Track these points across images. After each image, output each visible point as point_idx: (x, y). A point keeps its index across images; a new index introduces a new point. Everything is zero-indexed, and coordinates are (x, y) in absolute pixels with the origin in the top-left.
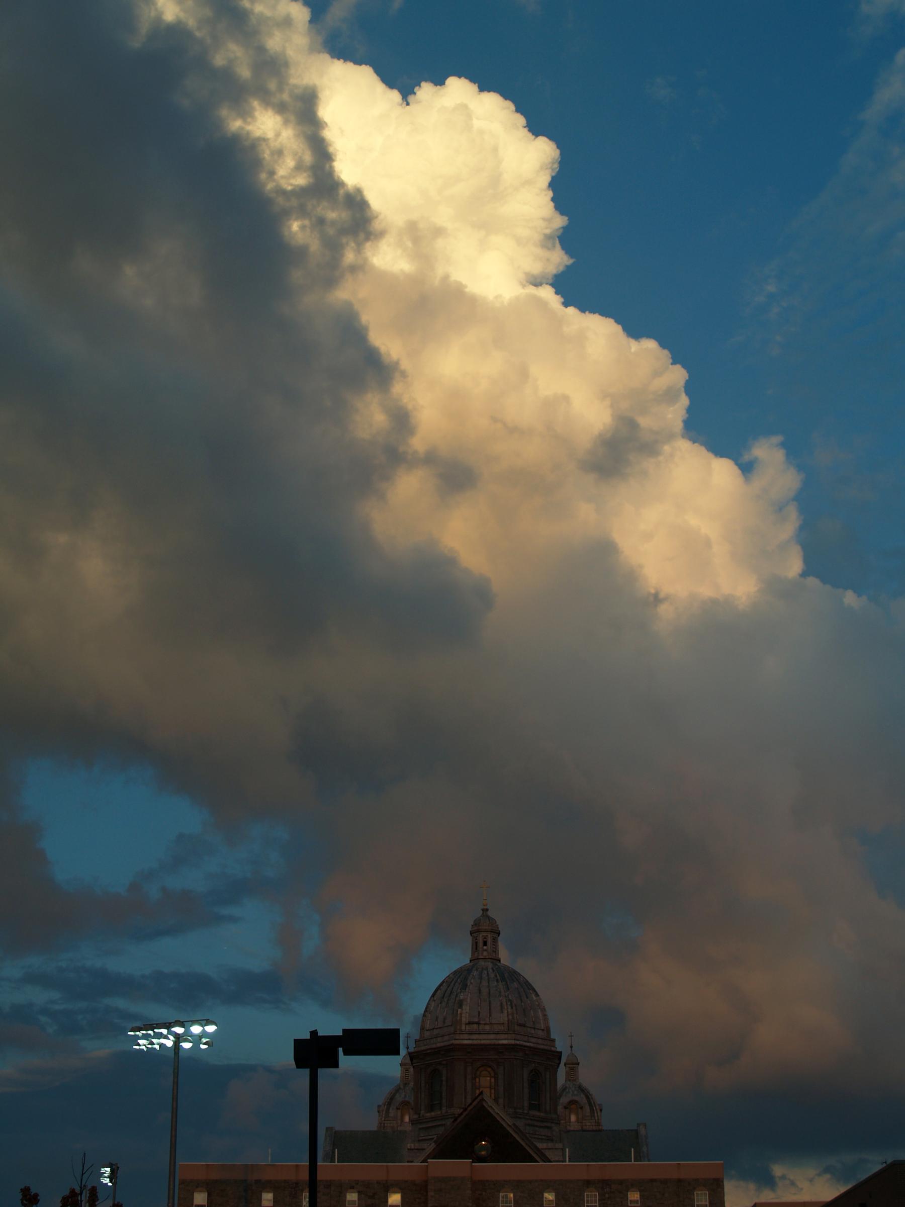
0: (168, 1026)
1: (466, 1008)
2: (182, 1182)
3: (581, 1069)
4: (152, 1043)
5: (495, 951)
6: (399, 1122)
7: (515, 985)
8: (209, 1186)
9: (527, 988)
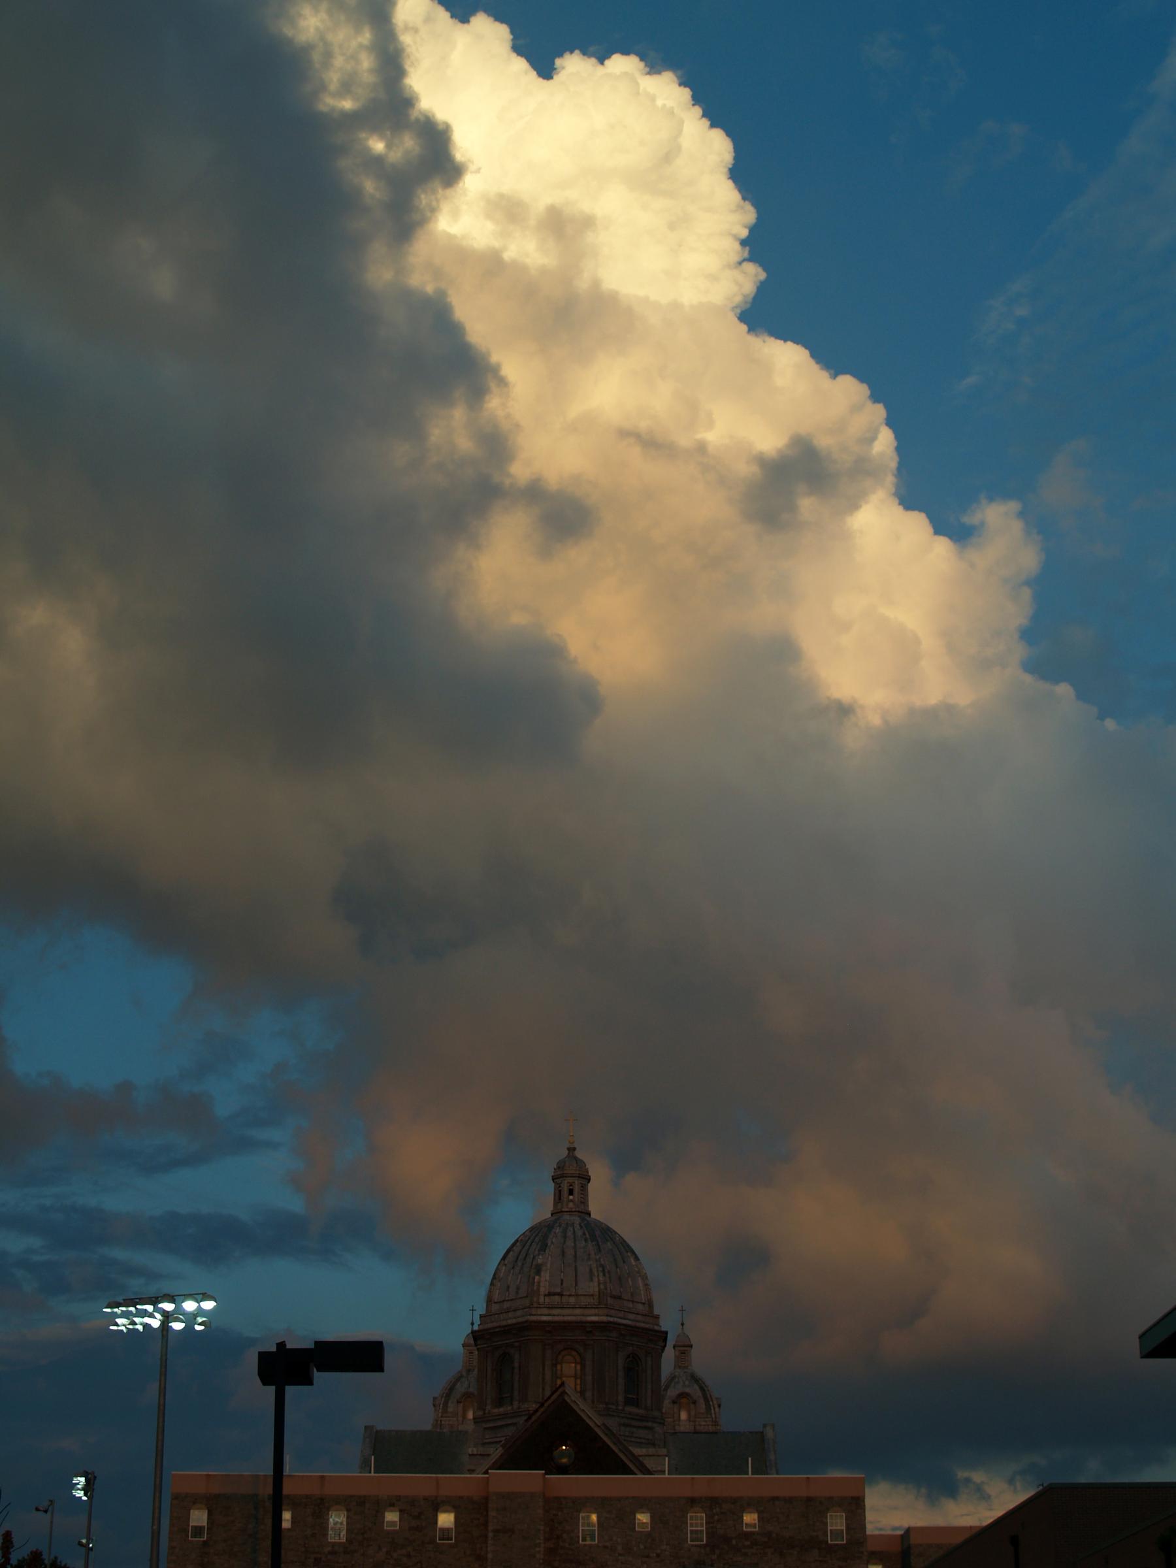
0: (154, 1301)
1: (545, 1275)
2: (176, 1497)
3: (694, 1353)
4: (134, 1323)
5: (584, 1201)
6: (460, 1419)
7: (609, 1245)
8: (212, 1503)
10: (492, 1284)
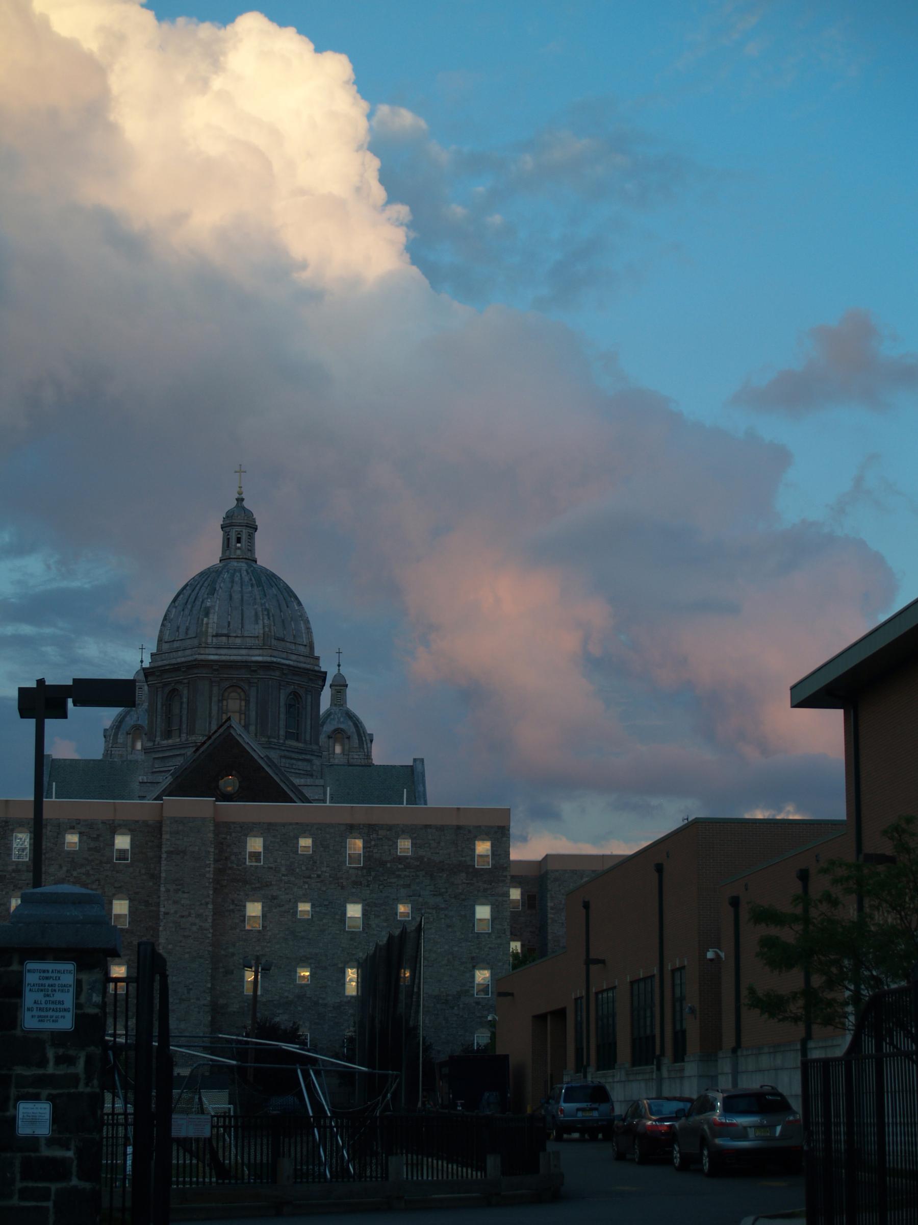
1: (214, 618)
5: (251, 549)
6: (129, 749)
10: (163, 625)
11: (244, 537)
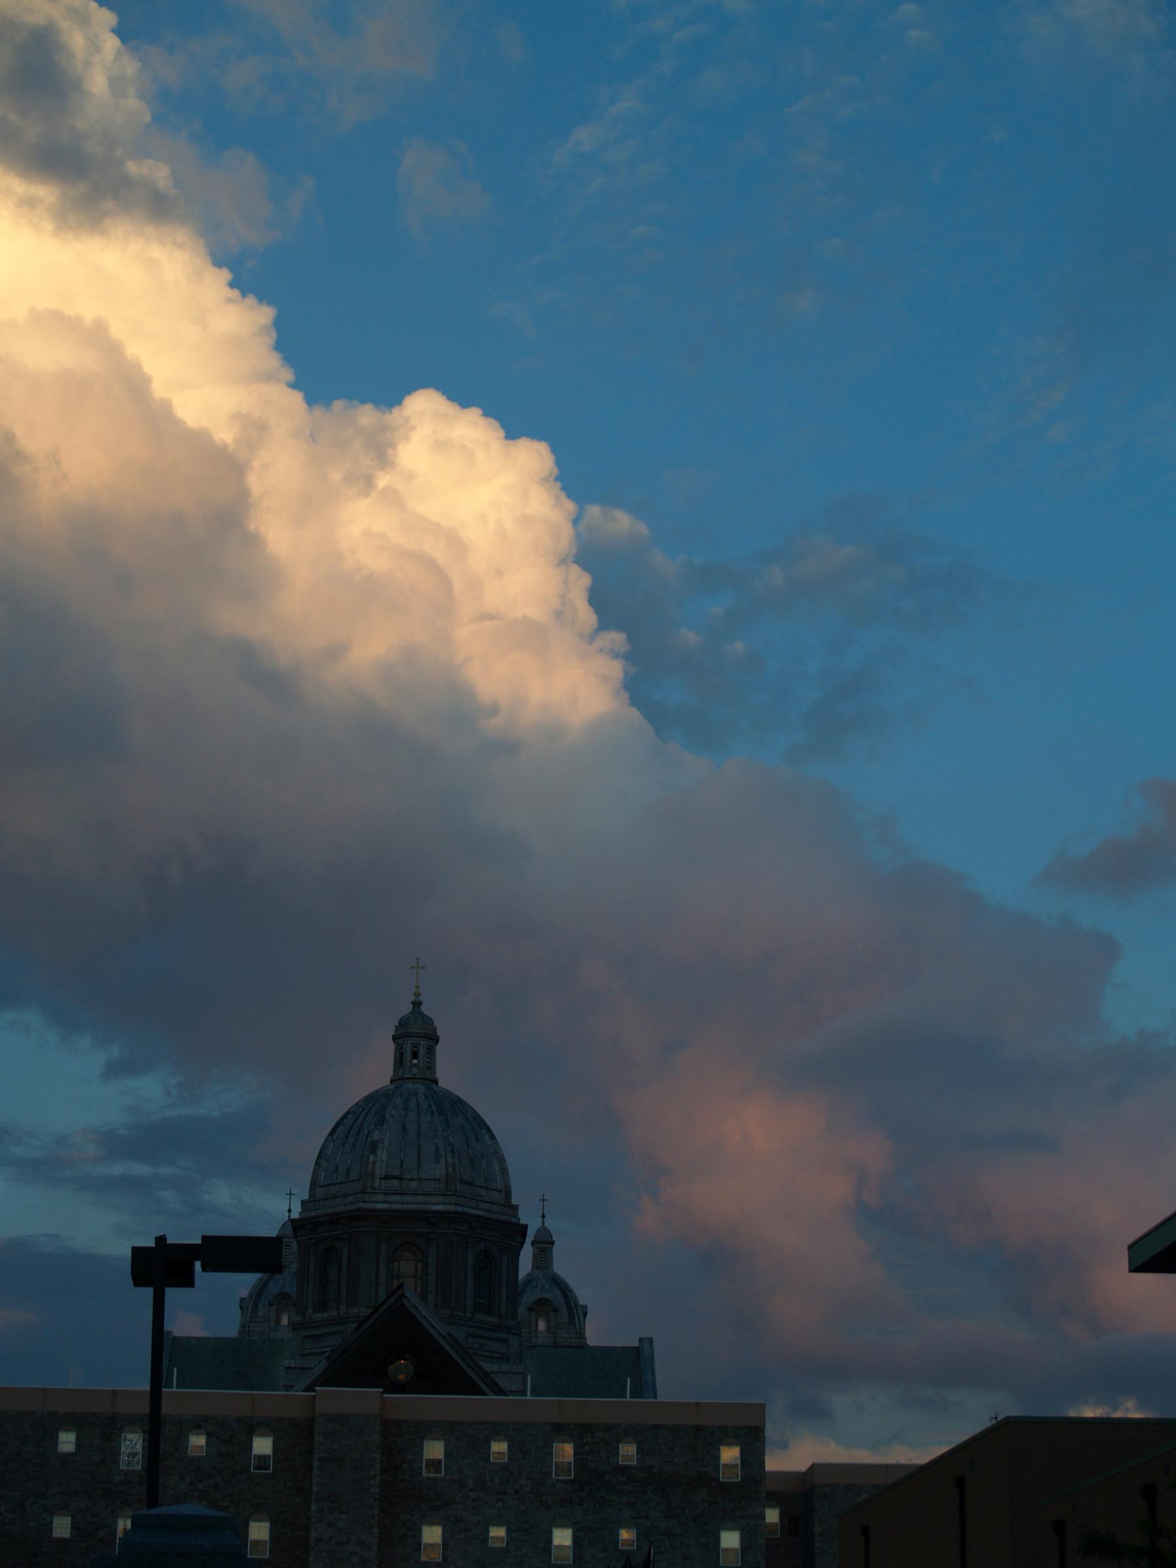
1: (382, 1155)
5: (431, 1067)
9: (479, 1125)
10: (317, 1164)
11: (422, 1051)
